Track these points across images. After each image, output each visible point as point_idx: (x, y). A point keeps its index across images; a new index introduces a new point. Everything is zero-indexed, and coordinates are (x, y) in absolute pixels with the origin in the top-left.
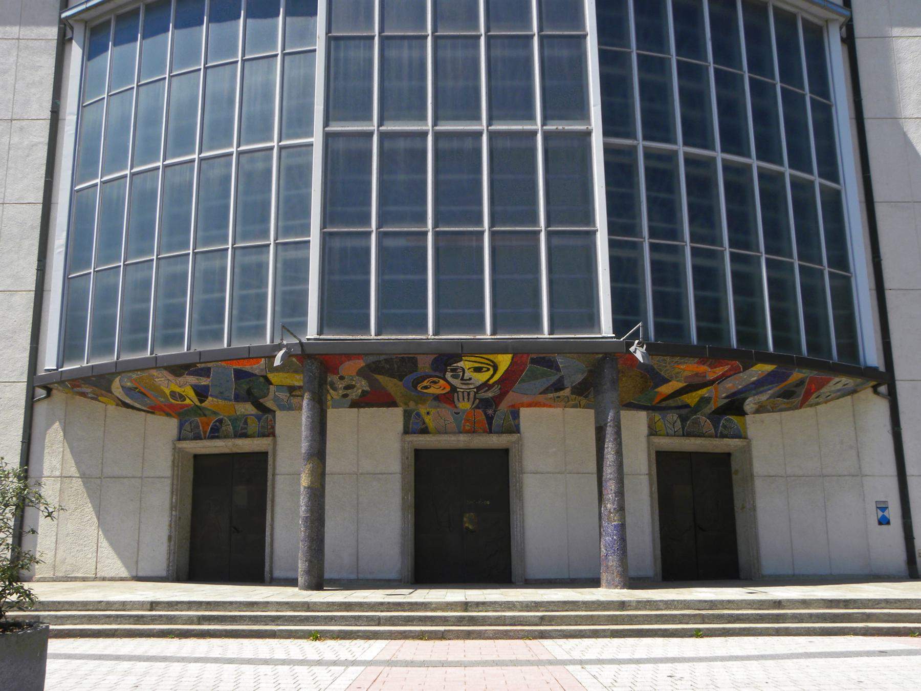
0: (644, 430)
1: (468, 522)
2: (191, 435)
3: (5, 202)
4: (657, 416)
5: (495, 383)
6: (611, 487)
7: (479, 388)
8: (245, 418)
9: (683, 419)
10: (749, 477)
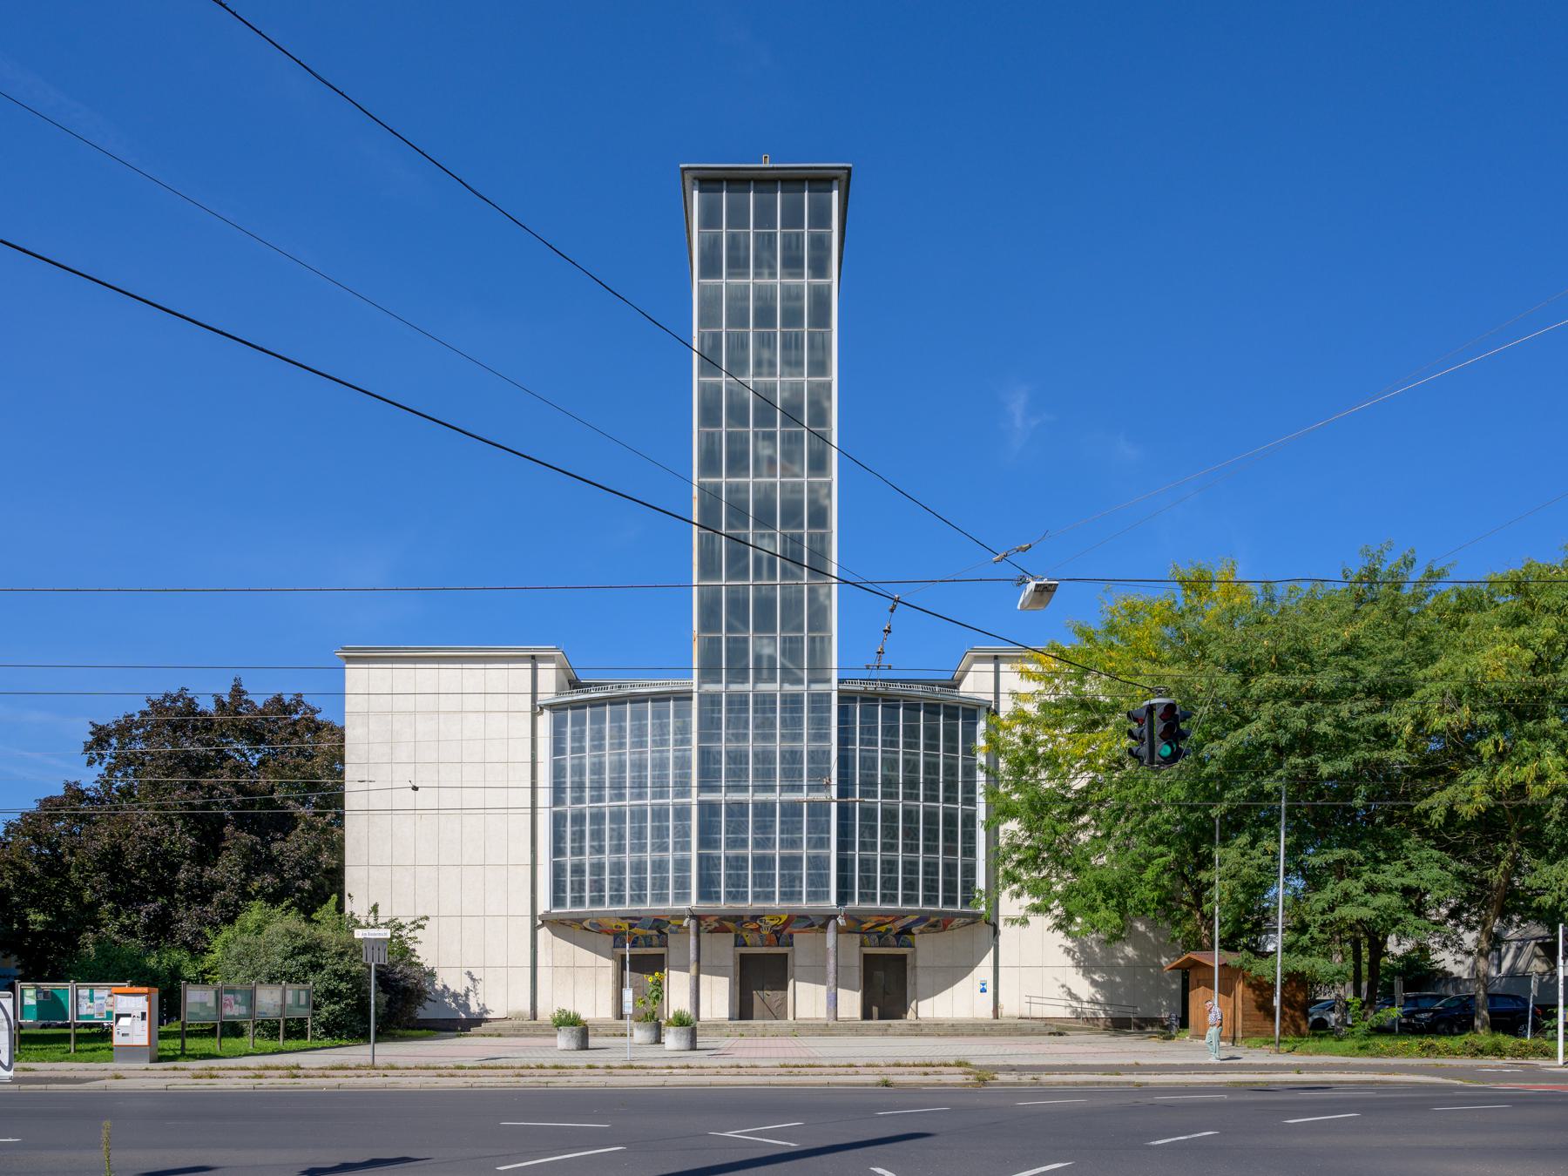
3: (505, 918)
4: (865, 937)
9: (880, 938)
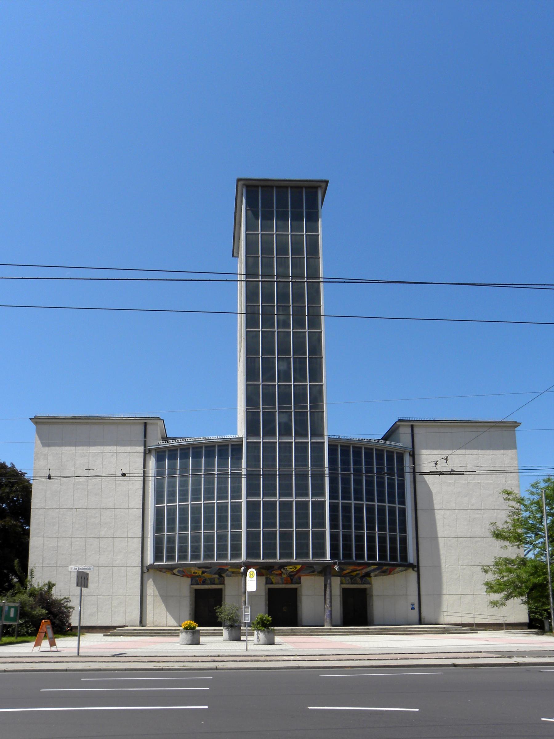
0: (339, 582)
1: (285, 609)
2: (195, 583)
4: (343, 578)
5: (296, 571)
6: (328, 601)
7: (290, 572)
8: (214, 579)
9: (351, 579)
10: (372, 596)
